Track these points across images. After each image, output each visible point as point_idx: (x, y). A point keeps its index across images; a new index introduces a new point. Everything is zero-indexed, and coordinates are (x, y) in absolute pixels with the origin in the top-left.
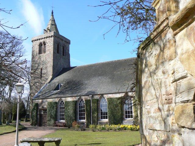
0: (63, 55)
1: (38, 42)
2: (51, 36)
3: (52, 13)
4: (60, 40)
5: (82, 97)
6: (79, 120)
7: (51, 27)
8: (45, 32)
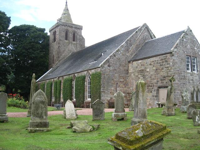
3: (66, 3)
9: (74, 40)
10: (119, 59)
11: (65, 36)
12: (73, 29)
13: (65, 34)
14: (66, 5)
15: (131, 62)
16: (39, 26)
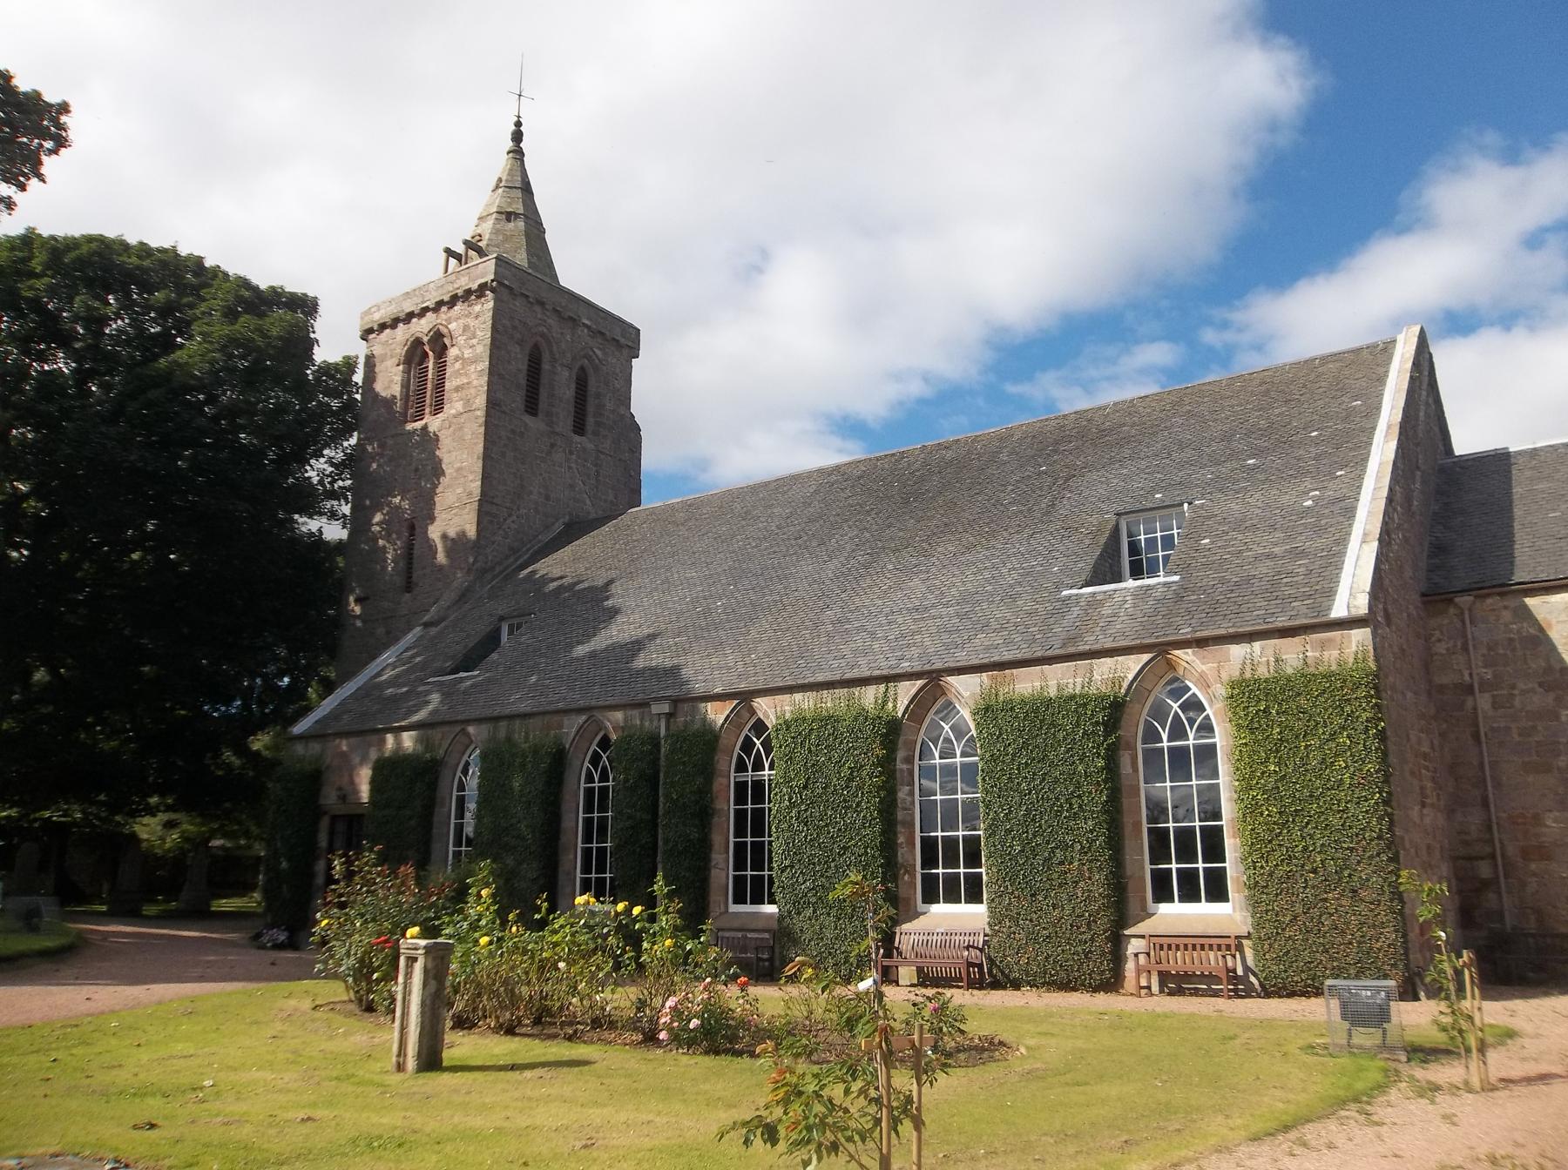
0: (579, 428)
1: (402, 334)
2: (481, 290)
3: (518, 136)
4: (552, 321)
5: (598, 715)
6: (735, 908)
7: (496, 232)
8: (453, 261)
11: (523, 382)
13: (524, 367)
14: (517, 153)
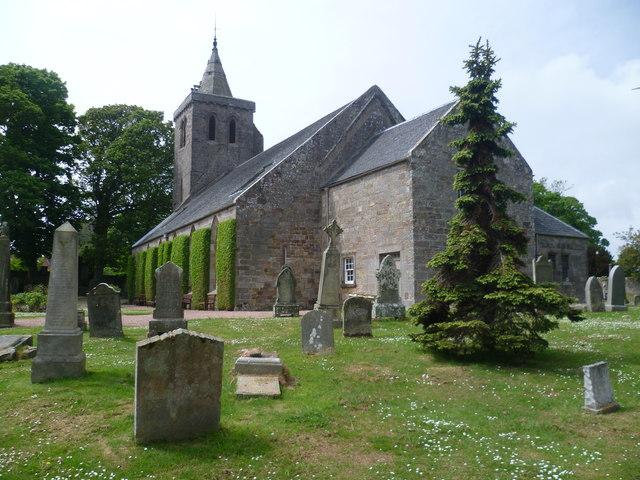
3: (215, 44)
9: (232, 140)
10: (294, 182)
12: (232, 111)
14: (215, 50)
15: (326, 189)
16: (149, 106)
